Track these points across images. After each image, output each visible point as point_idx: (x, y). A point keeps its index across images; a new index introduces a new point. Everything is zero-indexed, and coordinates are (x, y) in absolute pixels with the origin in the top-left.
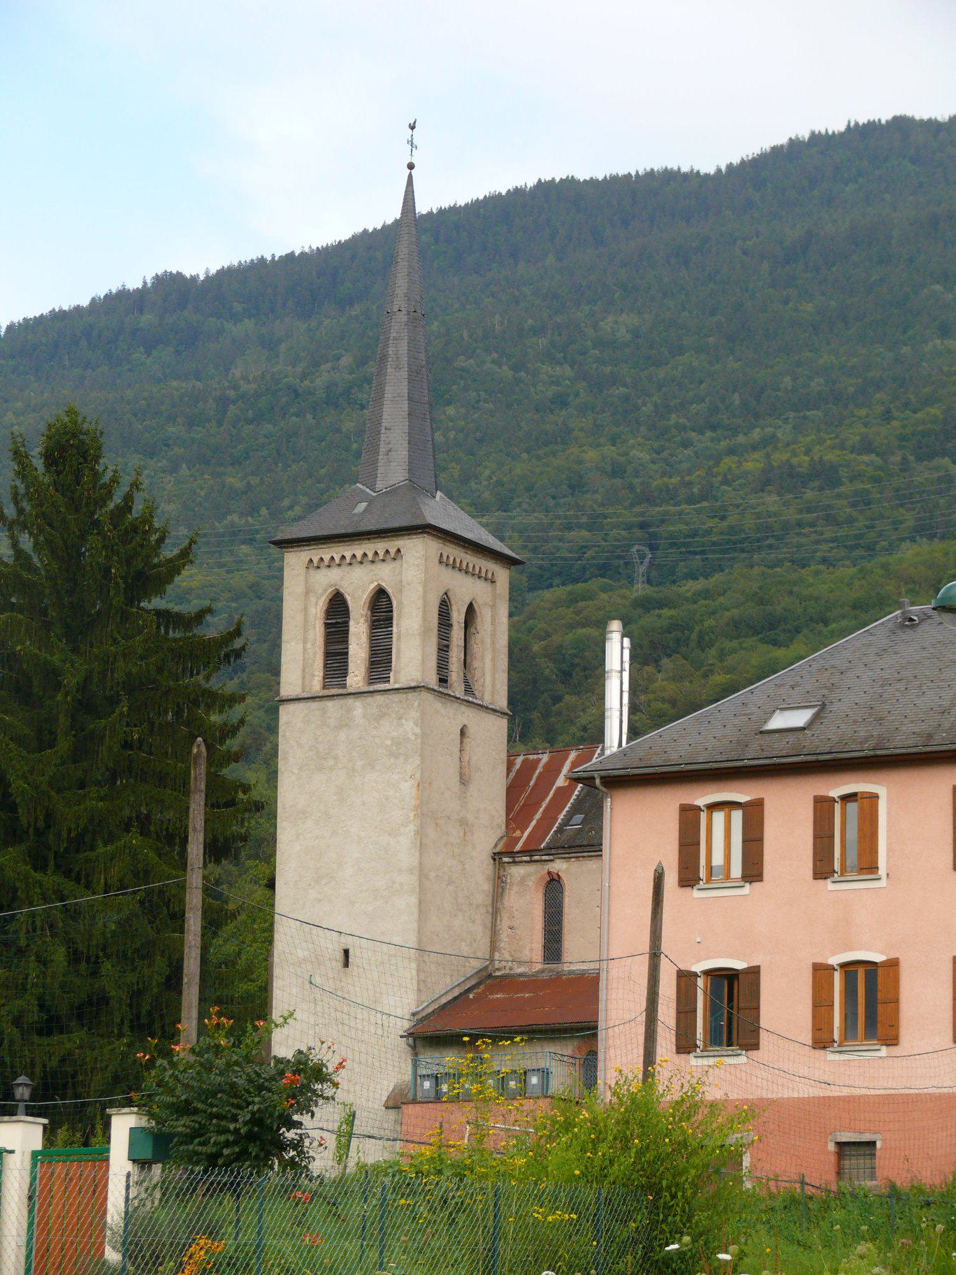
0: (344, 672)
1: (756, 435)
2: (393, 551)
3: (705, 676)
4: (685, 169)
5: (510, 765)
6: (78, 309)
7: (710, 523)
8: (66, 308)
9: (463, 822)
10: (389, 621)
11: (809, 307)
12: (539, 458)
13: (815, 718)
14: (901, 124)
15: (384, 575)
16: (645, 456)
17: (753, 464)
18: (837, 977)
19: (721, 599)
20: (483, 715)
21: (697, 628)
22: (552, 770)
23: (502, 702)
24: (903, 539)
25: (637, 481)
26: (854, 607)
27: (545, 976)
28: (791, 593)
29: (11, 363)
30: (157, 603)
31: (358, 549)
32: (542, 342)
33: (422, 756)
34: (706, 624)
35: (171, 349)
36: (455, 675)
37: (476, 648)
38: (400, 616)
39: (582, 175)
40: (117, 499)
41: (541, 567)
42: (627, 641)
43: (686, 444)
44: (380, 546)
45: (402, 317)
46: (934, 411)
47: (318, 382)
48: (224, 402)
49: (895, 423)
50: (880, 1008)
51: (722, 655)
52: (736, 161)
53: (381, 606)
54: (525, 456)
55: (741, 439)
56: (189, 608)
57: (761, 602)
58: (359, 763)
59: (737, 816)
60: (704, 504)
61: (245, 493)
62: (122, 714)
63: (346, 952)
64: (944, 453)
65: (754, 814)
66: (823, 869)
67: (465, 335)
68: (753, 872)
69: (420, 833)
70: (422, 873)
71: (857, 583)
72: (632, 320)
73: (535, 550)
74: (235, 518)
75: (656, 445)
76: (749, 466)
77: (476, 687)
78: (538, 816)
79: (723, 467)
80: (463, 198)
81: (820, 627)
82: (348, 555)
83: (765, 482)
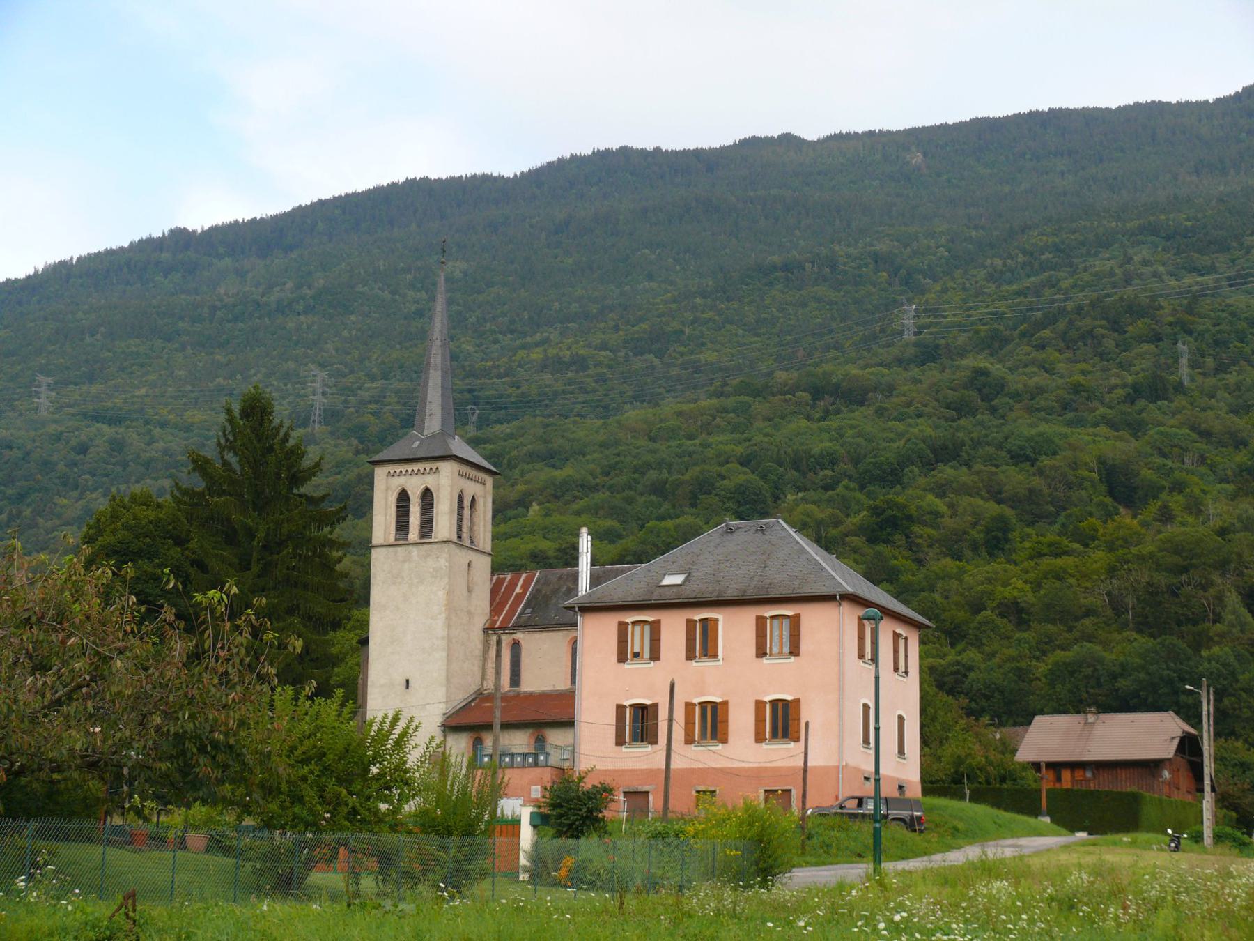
0: (407, 533)
1: (538, 337)
2: (434, 469)
3: (513, 486)
4: (495, 174)
5: (492, 580)
6: (122, 249)
7: (510, 391)
8: (114, 248)
9: (469, 612)
10: (431, 505)
11: (570, 261)
12: (407, 348)
13: (686, 579)
14: (625, 151)
15: (429, 481)
16: (471, 349)
17: (536, 355)
18: (697, 709)
19: (521, 439)
20: (479, 555)
21: (507, 457)
22: (513, 584)
23: (488, 548)
24: (626, 403)
25: (466, 364)
26: (601, 446)
27: (511, 694)
28: (563, 436)
29: (80, 280)
30: (302, 490)
31: (416, 467)
32: (409, 277)
33: (449, 578)
34: (512, 454)
35: (180, 275)
36: (465, 535)
37: (475, 520)
38: (438, 502)
39: (433, 176)
40: (282, 434)
41: (408, 415)
42: (589, 537)
43: (496, 342)
44: (428, 466)
45: (438, 343)
46: (645, 326)
47: (272, 298)
48: (214, 309)
49: (621, 333)
50: (719, 725)
51: (522, 474)
52: (526, 170)
53: (427, 498)
54: (398, 346)
55: (529, 339)
56: (317, 494)
57: (546, 442)
58: (415, 581)
59: (647, 629)
60: (507, 379)
61: (227, 365)
62: (288, 553)
63: (407, 681)
64: (650, 352)
65: (655, 627)
66: (690, 656)
67: (362, 272)
68: (655, 656)
69: (448, 618)
70: (449, 639)
71: (602, 431)
72: (463, 265)
73: (404, 404)
74: (220, 380)
75: (478, 342)
76: (534, 356)
77: (475, 541)
78: (507, 608)
79: (518, 357)
80: (360, 188)
81: (580, 457)
82: (410, 470)
83: (543, 367)
